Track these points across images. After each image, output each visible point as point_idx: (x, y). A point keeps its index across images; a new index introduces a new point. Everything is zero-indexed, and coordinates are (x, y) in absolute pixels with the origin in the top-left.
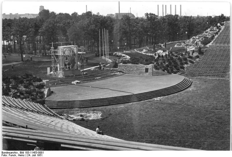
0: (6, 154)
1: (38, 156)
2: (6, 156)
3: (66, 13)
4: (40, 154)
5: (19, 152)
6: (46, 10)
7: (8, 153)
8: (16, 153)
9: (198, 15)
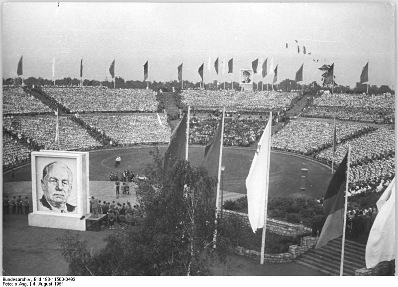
0: (9, 282)
1: (56, 286)
2: (10, 286)
4: (59, 282)
5: (32, 278)
7: (14, 280)
8: (27, 280)
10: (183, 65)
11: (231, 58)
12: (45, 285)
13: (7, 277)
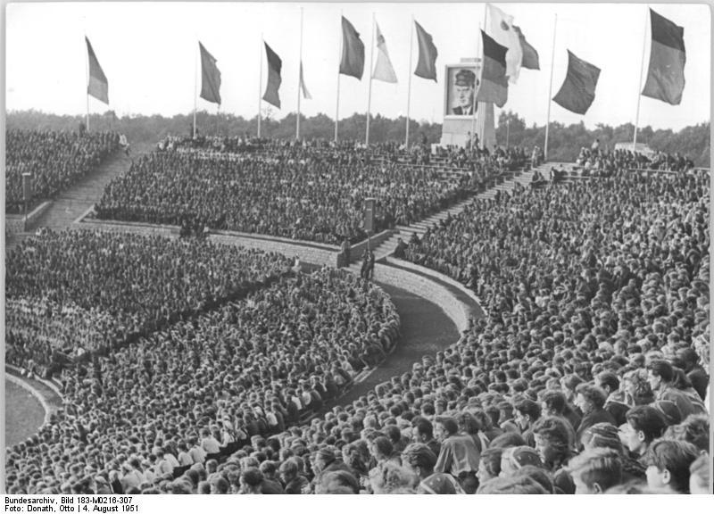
0: (17, 505)
1: (125, 512)
2: (17, 512)
3: (157, 113)
6: (59, 118)
7: (25, 501)
9: (535, 124)
10: (571, 50)
11: (340, 18)
12: (105, 510)
13: (12, 497)
